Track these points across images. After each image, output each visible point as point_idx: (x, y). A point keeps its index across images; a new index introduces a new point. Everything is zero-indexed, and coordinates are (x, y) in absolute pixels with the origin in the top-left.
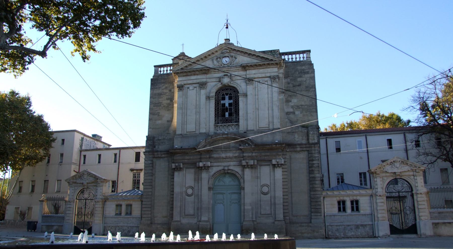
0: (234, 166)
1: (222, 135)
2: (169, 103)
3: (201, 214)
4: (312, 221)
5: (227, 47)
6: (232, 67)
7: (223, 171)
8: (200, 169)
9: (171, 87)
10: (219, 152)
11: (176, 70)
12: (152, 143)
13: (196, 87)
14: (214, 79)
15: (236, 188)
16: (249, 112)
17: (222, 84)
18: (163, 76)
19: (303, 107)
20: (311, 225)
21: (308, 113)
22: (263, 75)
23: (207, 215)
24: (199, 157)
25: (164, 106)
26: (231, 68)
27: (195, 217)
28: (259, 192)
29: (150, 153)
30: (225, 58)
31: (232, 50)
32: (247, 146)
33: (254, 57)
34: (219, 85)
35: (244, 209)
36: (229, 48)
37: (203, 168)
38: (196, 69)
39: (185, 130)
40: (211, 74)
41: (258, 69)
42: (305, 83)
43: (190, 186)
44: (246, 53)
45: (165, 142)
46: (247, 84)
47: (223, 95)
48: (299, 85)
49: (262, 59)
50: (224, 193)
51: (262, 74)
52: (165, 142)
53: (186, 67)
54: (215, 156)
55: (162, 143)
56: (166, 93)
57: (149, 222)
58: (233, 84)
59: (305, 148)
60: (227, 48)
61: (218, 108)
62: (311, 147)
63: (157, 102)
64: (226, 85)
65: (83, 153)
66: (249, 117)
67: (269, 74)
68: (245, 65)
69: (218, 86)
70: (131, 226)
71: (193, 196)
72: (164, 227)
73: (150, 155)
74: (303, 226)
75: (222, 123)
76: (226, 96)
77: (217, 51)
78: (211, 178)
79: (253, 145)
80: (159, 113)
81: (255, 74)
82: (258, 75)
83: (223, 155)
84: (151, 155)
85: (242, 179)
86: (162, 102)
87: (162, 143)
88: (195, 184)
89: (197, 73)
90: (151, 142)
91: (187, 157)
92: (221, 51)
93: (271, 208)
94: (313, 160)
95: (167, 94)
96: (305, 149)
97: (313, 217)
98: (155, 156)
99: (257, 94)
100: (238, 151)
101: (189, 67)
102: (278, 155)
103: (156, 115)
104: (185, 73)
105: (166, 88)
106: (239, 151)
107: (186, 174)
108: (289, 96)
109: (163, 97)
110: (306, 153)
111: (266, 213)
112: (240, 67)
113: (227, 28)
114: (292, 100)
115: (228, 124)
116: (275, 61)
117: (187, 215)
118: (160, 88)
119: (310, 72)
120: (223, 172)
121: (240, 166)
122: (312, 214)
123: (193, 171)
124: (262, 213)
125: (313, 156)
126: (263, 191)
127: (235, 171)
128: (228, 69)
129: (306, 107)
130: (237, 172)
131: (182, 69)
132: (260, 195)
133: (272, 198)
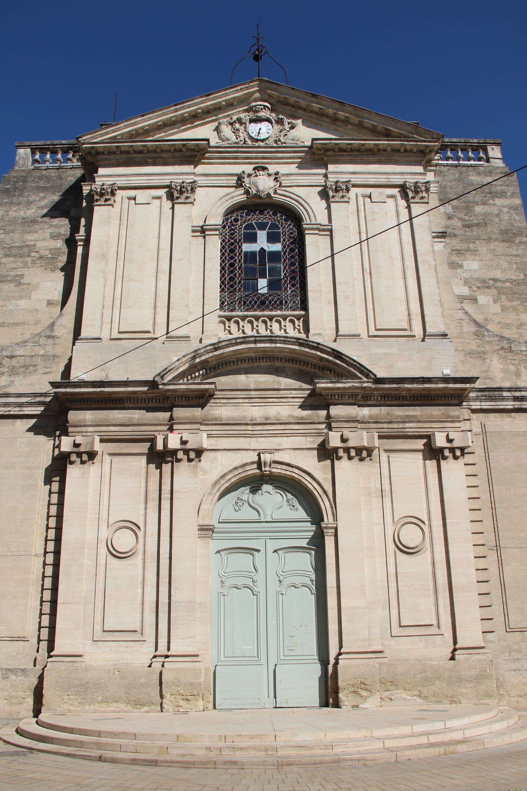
17: (247, 192)
19: (499, 284)
21: (514, 303)
25: (41, 257)
28: (391, 546)
34: (239, 196)
39: (115, 326)
42: (497, 220)
45: (35, 366)
47: (250, 226)
50: (258, 551)
61: (232, 265)
63: (16, 245)
65: (99, 634)
75: (247, 310)
80: (22, 276)
103: (11, 281)
108: (452, 250)
113: (257, 58)
114: (465, 264)
118: (30, 203)
119: (509, 194)
129: (508, 284)
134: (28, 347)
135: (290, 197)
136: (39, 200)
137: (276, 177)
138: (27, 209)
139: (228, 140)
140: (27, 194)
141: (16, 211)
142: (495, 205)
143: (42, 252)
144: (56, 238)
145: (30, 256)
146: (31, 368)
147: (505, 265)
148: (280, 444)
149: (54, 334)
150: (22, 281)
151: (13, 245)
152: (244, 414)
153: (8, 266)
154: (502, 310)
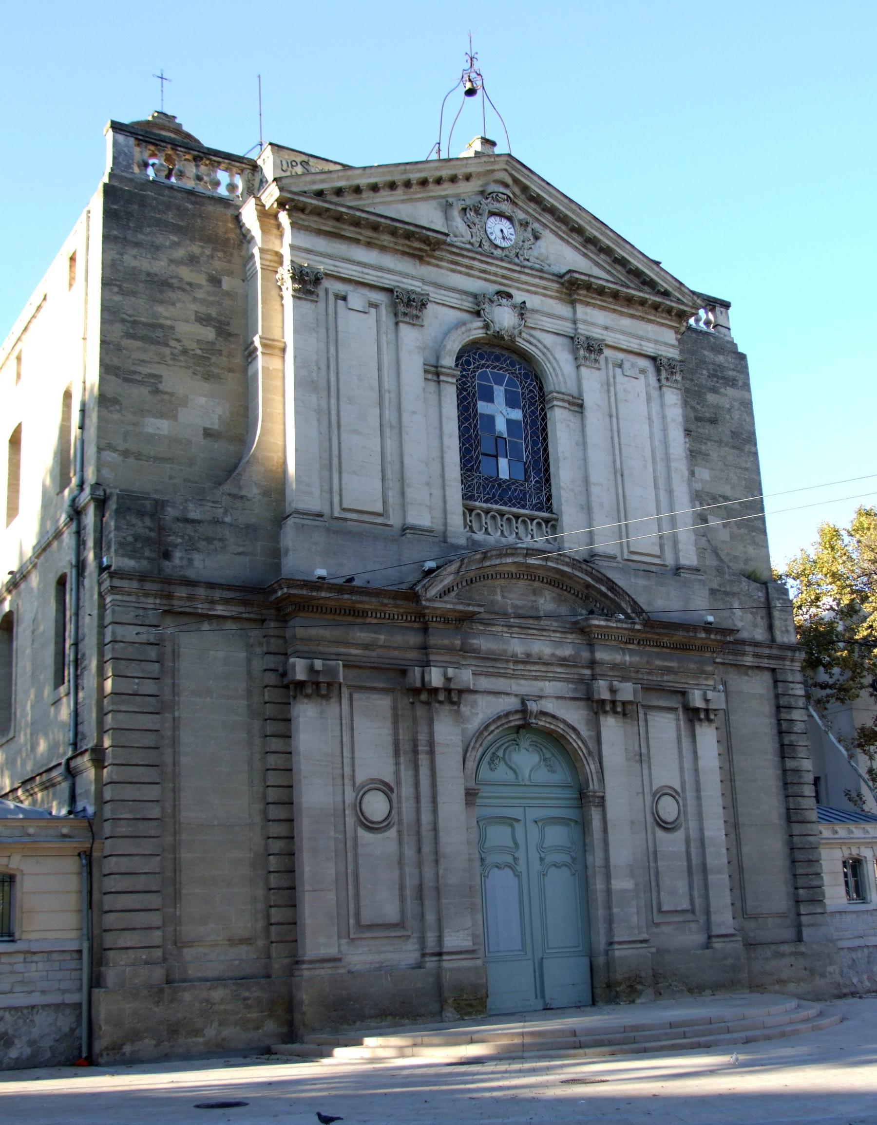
0: (560, 702)
1: (527, 555)
2: (213, 343)
3: (439, 920)
4: (806, 933)
5: (511, 175)
6: (527, 271)
7: (517, 716)
8: (424, 697)
9: (217, 264)
10: (500, 629)
11: (295, 189)
12: (151, 529)
13: (375, 306)
14: (452, 295)
15: (565, 799)
16: (594, 477)
17: (487, 326)
18: (166, 192)
20: (803, 949)
22: (634, 345)
23: (469, 924)
24: (414, 639)
25: (185, 352)
26: (520, 272)
27: (409, 937)
28: (650, 819)
29: (148, 586)
30: (498, 218)
31: (523, 197)
32: (620, 621)
33: (602, 259)
34: (475, 329)
35: (608, 891)
36: (516, 181)
37: (442, 697)
38: (388, 222)
40: (437, 266)
41: (614, 311)
42: (728, 417)
43: (373, 781)
44: (578, 230)
45: (221, 540)
46: (400, 318)
48: (713, 421)
49: (631, 277)
50: (518, 821)
51: (631, 340)
52: (221, 540)
53: (339, 192)
54: (483, 644)
55: (209, 540)
56: (190, 284)
57: (158, 974)
58: (531, 343)
59: (766, 661)
60: (509, 181)
62: (783, 658)
63: (143, 319)
64: (502, 338)
66: (594, 498)
67: (652, 345)
68: (583, 277)
69: (470, 330)
70: (16, 1009)
71: (393, 833)
72: (247, 994)
73: (147, 595)
74: (783, 955)
76: (495, 387)
77: (468, 178)
78: (473, 748)
79: (637, 620)
81: (606, 328)
82: (618, 336)
83: (517, 646)
84: (155, 596)
85: (591, 762)
86: (172, 328)
87: (209, 540)
88: (397, 773)
89: (386, 239)
90: (148, 522)
91: (362, 635)
92: (480, 182)
93: (691, 888)
94: (790, 708)
95: (200, 294)
96: (765, 663)
97: (804, 919)
98: (176, 602)
99: (614, 413)
100: (569, 636)
101: (350, 200)
102: (703, 672)
103: (141, 383)
104: (332, 223)
105: (192, 260)
106: (574, 636)
107: (356, 719)
109: (178, 305)
110: (767, 676)
111: (679, 909)
112: (553, 281)
115: (515, 510)
116: (679, 301)
117: (371, 927)
118: (158, 248)
120: (517, 723)
121: (578, 703)
122: (803, 909)
123: (383, 703)
124: (665, 908)
125: (791, 692)
126: (663, 817)
127: (564, 722)
128: (509, 270)
130: (574, 729)
131: (320, 194)
132: (654, 834)
133: (692, 845)
134: (206, 508)
135: (536, 346)
136: (170, 247)
137: (522, 310)
138: (153, 258)
139: (462, 236)
140: (148, 230)
141: (135, 257)
142: (726, 395)
143: (187, 343)
144: (204, 323)
145: (167, 345)
146: (216, 542)
147: (734, 479)
148: (542, 690)
149: (243, 493)
150: (161, 387)
151: (138, 319)
152: (505, 647)
153: (135, 355)
154: (731, 537)
